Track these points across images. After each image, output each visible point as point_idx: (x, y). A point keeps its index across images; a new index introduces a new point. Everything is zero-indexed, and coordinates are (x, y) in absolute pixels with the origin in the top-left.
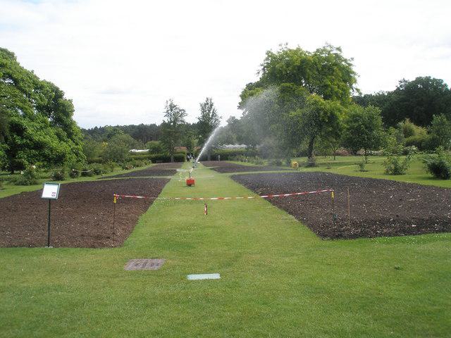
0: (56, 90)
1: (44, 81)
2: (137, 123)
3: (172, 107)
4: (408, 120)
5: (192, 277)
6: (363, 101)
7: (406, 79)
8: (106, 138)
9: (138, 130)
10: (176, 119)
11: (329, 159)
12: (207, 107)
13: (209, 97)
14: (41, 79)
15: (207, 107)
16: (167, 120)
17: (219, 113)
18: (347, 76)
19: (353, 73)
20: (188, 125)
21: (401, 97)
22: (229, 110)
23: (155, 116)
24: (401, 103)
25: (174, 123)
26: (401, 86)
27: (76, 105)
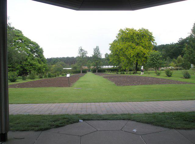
0: (37, 44)
1: (32, 41)
2: (66, 57)
3: (81, 50)
4: (180, 56)
5: (71, 68)
6: (156, 48)
7: (182, 38)
8: (53, 63)
9: (132, 32)
10: (83, 56)
11: (182, 81)
12: (97, 50)
13: (98, 46)
14: (32, 41)
15: (97, 50)
16: (79, 55)
17: (101, 52)
18: (151, 38)
19: (153, 37)
20: (88, 57)
21: (180, 45)
22: (105, 51)
23: (74, 54)
24: (180, 48)
25: (83, 57)
26: (180, 41)
27: (44, 50)
